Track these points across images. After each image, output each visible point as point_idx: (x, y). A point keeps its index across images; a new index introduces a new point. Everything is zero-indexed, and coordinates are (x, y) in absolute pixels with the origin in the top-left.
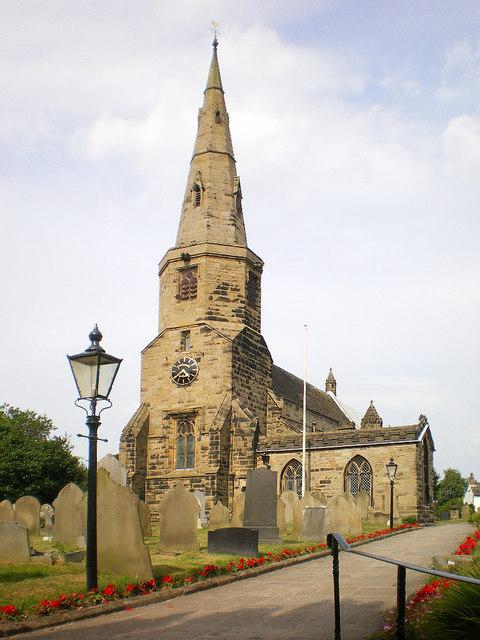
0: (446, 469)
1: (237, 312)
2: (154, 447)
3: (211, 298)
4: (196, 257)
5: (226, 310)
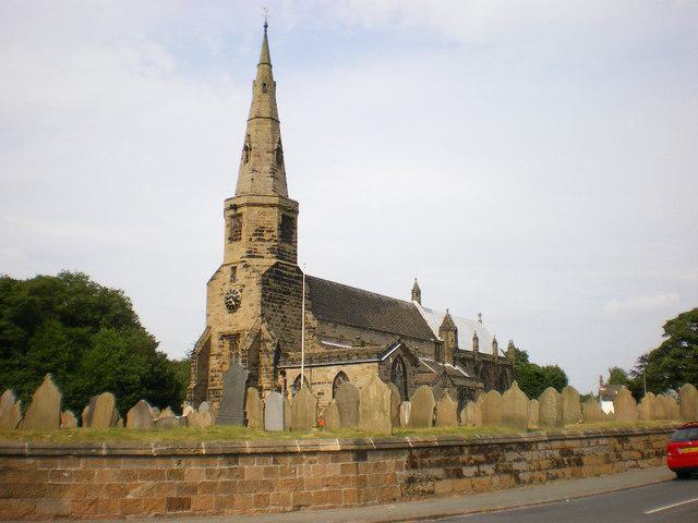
0: (612, 366)
1: (271, 250)
2: (214, 363)
3: (251, 240)
4: (242, 206)
5: (263, 249)
